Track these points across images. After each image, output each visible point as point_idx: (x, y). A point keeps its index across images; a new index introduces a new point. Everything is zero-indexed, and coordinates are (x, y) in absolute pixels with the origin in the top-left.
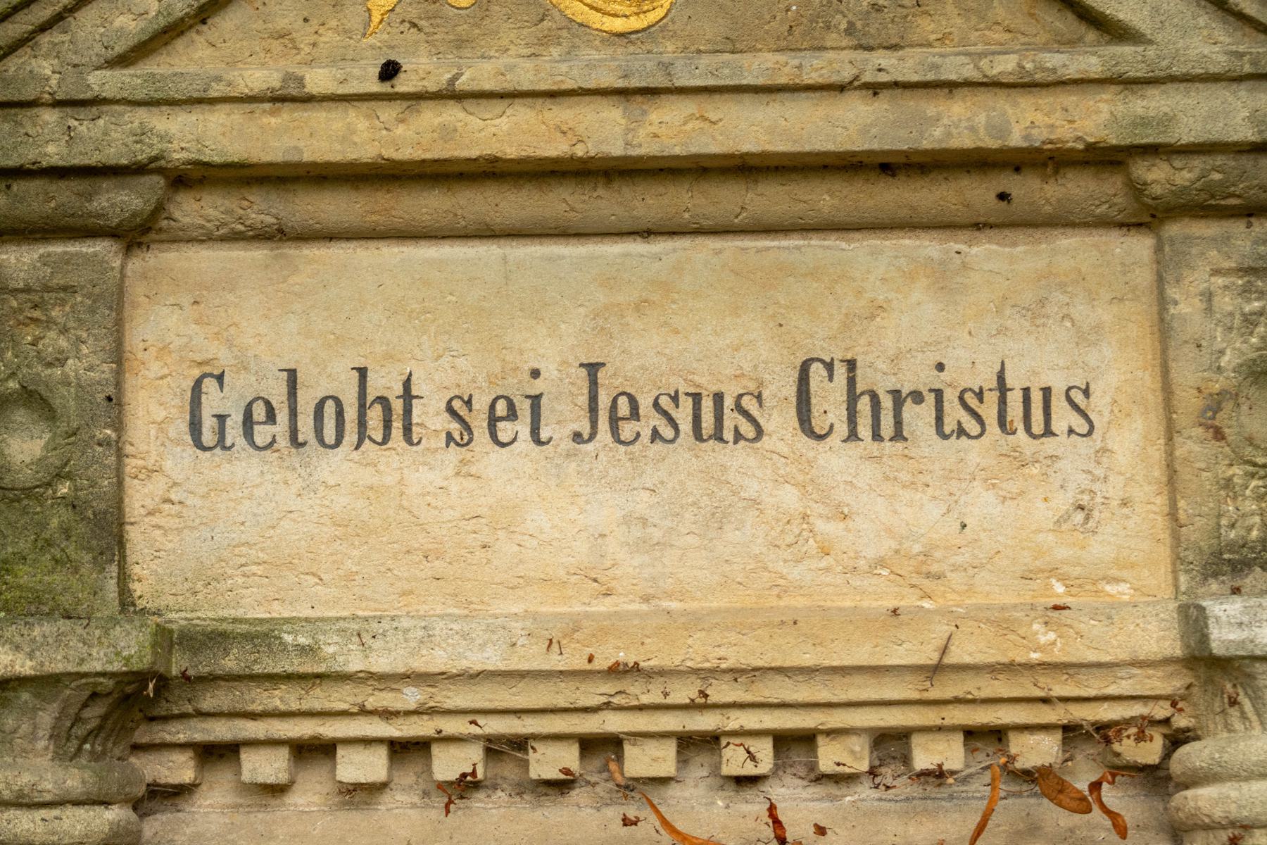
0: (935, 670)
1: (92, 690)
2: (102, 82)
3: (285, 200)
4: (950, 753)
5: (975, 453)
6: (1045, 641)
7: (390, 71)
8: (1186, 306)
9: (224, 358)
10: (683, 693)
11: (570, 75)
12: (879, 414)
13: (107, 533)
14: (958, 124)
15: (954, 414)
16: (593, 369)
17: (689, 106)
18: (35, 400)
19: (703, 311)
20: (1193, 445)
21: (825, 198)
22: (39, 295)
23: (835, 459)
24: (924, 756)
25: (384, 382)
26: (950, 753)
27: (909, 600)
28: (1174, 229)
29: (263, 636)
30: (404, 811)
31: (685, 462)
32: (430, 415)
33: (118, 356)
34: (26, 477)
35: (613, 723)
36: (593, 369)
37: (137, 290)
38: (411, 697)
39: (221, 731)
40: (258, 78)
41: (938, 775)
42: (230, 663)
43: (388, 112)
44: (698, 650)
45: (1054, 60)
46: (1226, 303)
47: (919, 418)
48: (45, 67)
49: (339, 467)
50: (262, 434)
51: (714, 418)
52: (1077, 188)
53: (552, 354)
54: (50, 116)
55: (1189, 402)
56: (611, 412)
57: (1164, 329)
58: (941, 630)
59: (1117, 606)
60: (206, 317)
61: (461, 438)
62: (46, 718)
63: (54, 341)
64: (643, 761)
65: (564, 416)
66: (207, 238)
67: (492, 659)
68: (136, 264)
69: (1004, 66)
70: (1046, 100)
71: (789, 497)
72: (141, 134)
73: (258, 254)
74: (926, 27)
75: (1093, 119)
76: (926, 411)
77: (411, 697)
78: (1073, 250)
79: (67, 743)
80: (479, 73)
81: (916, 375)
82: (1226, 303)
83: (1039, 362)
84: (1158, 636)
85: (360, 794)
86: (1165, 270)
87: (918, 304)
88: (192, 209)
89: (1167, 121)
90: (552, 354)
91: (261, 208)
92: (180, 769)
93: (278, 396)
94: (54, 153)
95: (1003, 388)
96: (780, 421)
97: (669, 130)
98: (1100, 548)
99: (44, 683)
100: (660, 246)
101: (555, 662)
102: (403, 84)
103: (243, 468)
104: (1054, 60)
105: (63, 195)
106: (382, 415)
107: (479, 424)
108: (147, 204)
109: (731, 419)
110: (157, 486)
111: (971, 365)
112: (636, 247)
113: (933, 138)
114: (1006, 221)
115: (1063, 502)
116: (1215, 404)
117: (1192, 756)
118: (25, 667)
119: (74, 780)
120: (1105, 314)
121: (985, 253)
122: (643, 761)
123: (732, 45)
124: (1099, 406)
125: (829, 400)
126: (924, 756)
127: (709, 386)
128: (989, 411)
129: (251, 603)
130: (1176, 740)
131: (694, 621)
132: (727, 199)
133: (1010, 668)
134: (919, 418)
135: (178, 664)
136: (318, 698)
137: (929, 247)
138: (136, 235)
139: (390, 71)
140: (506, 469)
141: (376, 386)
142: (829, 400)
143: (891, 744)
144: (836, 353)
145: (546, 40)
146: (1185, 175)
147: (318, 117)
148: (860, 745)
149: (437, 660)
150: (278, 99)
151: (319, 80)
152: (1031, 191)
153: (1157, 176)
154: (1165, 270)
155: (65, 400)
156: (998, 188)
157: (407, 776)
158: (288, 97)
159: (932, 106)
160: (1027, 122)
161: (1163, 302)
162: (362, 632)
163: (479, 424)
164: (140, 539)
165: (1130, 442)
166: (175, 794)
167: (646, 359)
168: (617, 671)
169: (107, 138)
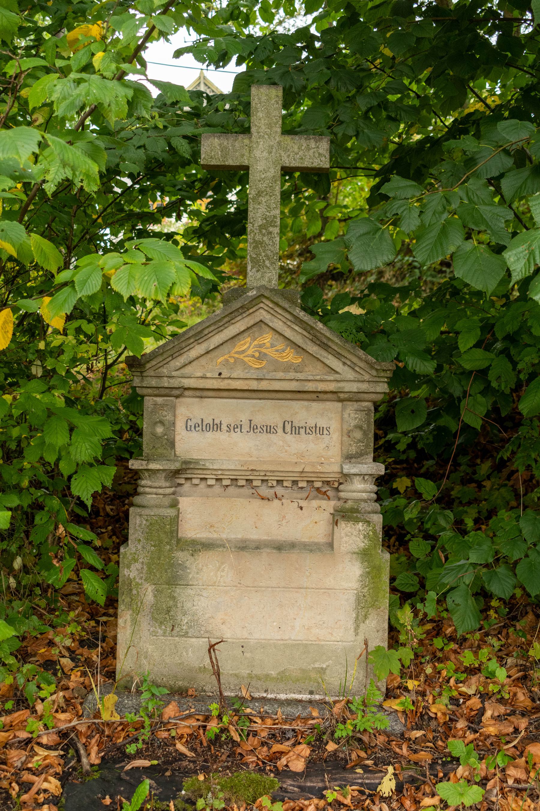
0: (302, 472)
1: (171, 471)
2: (174, 374)
3: (201, 393)
4: (304, 484)
5: (311, 437)
6: (319, 468)
7: (220, 374)
8: (346, 416)
9: (192, 417)
10: (263, 474)
11: (248, 376)
12: (296, 430)
13: (172, 444)
14: (310, 386)
15: (308, 430)
16: (250, 421)
17: (267, 382)
18: (162, 422)
19: (269, 413)
20: (345, 438)
21: (289, 396)
22: (162, 406)
23: (289, 437)
24: (300, 485)
25: (217, 421)
26: (304, 484)
27: (299, 460)
28: (345, 403)
29: (197, 462)
30: (218, 489)
31: (265, 436)
32: (224, 427)
33: (175, 416)
34: (160, 435)
35: (251, 478)
36: (250, 421)
37: (178, 405)
38: (220, 472)
39: (189, 476)
40: (199, 374)
41: (302, 488)
42: (192, 466)
43: (219, 380)
44: (265, 467)
45: (326, 377)
46: (352, 415)
47: (302, 431)
48: (165, 371)
49: (210, 435)
50: (197, 429)
51: (269, 430)
52: (329, 396)
53: (244, 418)
54: (165, 379)
55: (345, 431)
56: (253, 428)
57: (342, 419)
58: (303, 466)
59: (331, 463)
60: (188, 410)
61: (229, 431)
62: (164, 475)
63: (165, 413)
64: (255, 483)
65: (246, 428)
66: (189, 397)
67: (233, 467)
68: (178, 400)
69: (318, 378)
70: (324, 383)
71: (281, 443)
72: (180, 382)
73: (197, 399)
74: (306, 369)
75: (332, 387)
76: (304, 430)
77: (220, 472)
78: (329, 405)
79: (166, 479)
80: (234, 375)
81: (302, 424)
82: (352, 415)
83: (322, 423)
84: (337, 469)
85: (210, 486)
86: (344, 409)
87: (304, 413)
88: (187, 393)
89: (344, 388)
90: (244, 418)
91: (198, 393)
92: (182, 481)
93: (200, 423)
94: (166, 385)
95: (316, 427)
96: (280, 431)
97: (264, 385)
98: (330, 453)
99: (164, 470)
100: (262, 401)
101: (243, 468)
102: (222, 376)
103: (194, 434)
104: (326, 377)
105: (167, 391)
106: (216, 427)
107: (232, 429)
108: (181, 392)
109: (272, 430)
110: (180, 436)
111: (311, 423)
112: (259, 401)
113: (306, 389)
114: (318, 399)
115: (325, 445)
116: (349, 432)
117: (341, 487)
118: (161, 468)
119: (168, 484)
120: (333, 416)
121: (314, 405)
122: (255, 483)
123: (275, 371)
124: (331, 430)
125: (288, 427)
126: (300, 485)
127: (269, 424)
128: (313, 430)
129: (195, 456)
130: (340, 484)
131: (264, 462)
132: (274, 395)
133: (314, 472)
134: (302, 431)
135: (184, 466)
136: (205, 472)
137: (306, 403)
138: (177, 397)
139: (220, 374)
140: (236, 436)
141: (216, 422)
142: (288, 427)
143: (295, 482)
144: (290, 420)
145: (245, 369)
146: (346, 396)
147: (208, 380)
148: (290, 483)
149: (224, 467)
150: (202, 377)
151: (209, 375)
152: (321, 396)
153: (342, 396)
154: (344, 409)
155: (166, 423)
156: (318, 396)
157: (218, 483)
158: (204, 377)
159: (306, 383)
160: (321, 387)
161: (342, 415)
162: (212, 461)
163: (232, 429)
164: (177, 445)
165: (336, 436)
166: (180, 485)
167: (259, 420)
168: (252, 470)
169: (175, 383)
